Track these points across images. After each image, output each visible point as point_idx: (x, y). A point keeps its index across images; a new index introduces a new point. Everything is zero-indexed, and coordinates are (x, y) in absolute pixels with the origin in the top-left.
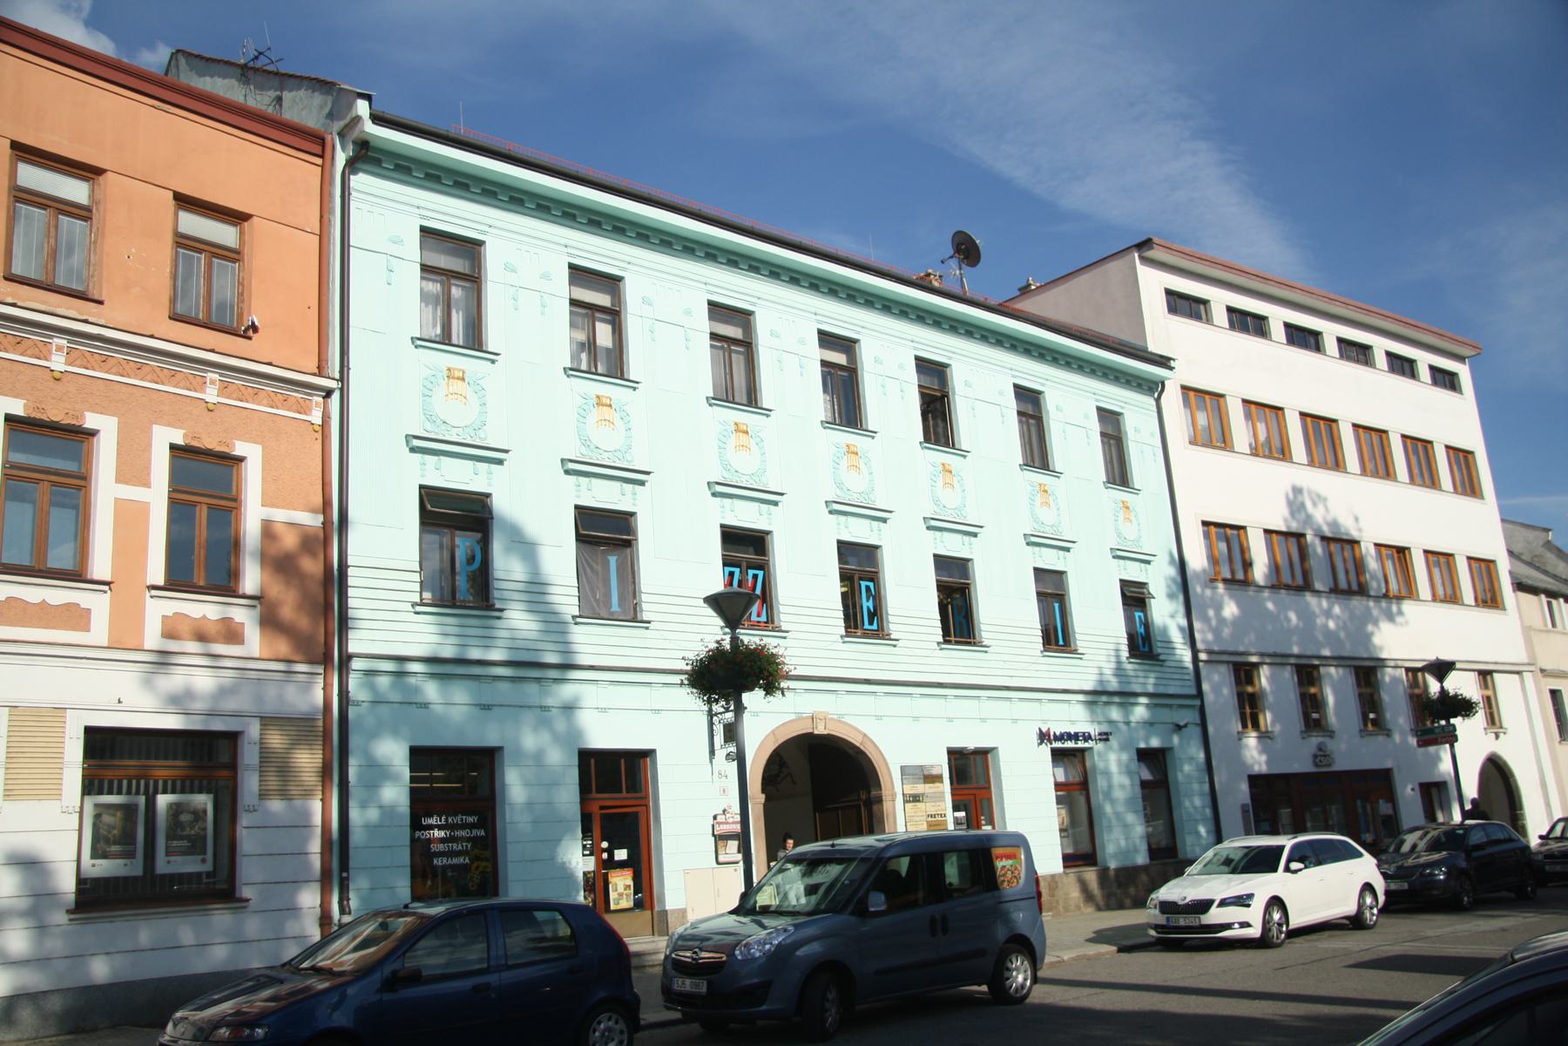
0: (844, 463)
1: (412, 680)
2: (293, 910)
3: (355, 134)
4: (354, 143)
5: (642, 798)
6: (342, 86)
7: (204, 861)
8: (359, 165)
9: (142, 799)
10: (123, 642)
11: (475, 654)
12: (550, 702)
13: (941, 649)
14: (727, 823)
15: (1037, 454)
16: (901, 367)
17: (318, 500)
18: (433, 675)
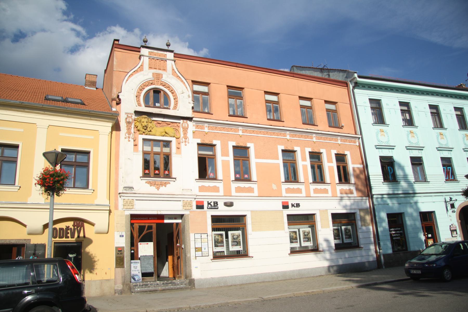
0: (440, 137)
1: (385, 199)
2: (369, 249)
3: (355, 81)
4: (354, 83)
5: (432, 222)
6: (350, 71)
7: (240, 247)
8: (355, 88)
9: (340, 227)
10: (334, 196)
11: (396, 192)
12: (412, 201)
13: (446, 183)
14: (453, 227)
15: (409, 122)
16: (425, 108)
17: (361, 161)
18: (389, 198)
